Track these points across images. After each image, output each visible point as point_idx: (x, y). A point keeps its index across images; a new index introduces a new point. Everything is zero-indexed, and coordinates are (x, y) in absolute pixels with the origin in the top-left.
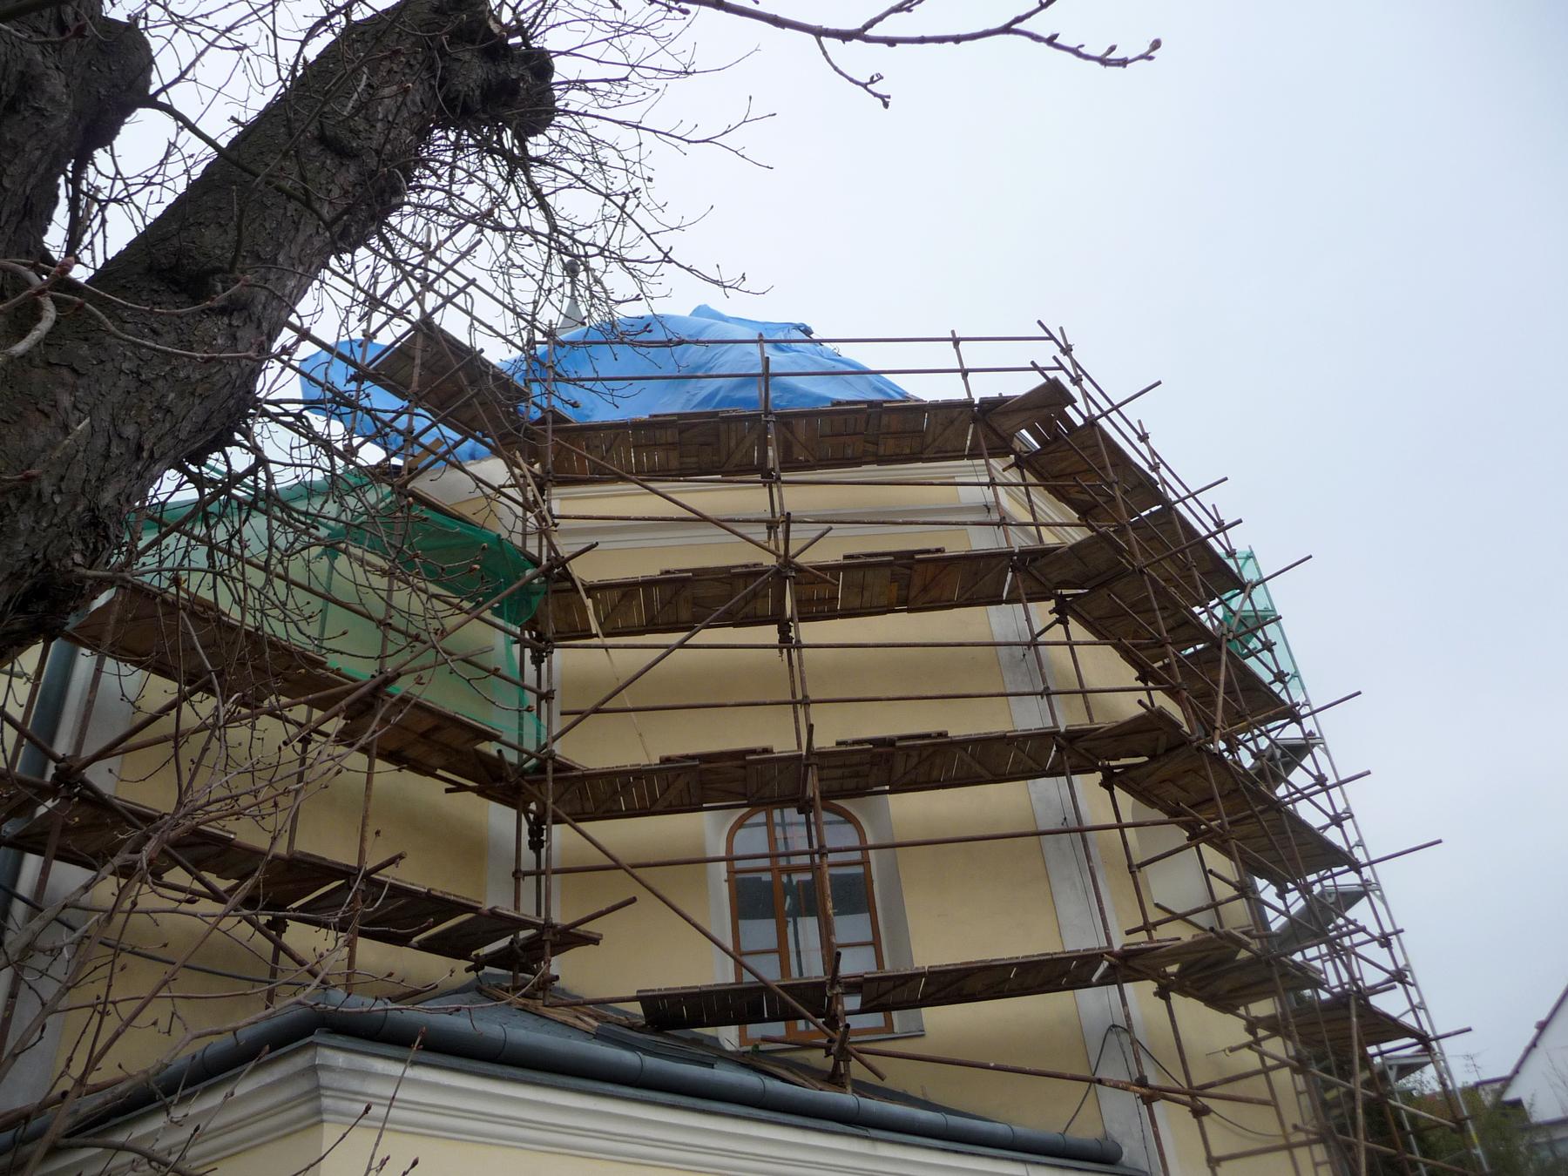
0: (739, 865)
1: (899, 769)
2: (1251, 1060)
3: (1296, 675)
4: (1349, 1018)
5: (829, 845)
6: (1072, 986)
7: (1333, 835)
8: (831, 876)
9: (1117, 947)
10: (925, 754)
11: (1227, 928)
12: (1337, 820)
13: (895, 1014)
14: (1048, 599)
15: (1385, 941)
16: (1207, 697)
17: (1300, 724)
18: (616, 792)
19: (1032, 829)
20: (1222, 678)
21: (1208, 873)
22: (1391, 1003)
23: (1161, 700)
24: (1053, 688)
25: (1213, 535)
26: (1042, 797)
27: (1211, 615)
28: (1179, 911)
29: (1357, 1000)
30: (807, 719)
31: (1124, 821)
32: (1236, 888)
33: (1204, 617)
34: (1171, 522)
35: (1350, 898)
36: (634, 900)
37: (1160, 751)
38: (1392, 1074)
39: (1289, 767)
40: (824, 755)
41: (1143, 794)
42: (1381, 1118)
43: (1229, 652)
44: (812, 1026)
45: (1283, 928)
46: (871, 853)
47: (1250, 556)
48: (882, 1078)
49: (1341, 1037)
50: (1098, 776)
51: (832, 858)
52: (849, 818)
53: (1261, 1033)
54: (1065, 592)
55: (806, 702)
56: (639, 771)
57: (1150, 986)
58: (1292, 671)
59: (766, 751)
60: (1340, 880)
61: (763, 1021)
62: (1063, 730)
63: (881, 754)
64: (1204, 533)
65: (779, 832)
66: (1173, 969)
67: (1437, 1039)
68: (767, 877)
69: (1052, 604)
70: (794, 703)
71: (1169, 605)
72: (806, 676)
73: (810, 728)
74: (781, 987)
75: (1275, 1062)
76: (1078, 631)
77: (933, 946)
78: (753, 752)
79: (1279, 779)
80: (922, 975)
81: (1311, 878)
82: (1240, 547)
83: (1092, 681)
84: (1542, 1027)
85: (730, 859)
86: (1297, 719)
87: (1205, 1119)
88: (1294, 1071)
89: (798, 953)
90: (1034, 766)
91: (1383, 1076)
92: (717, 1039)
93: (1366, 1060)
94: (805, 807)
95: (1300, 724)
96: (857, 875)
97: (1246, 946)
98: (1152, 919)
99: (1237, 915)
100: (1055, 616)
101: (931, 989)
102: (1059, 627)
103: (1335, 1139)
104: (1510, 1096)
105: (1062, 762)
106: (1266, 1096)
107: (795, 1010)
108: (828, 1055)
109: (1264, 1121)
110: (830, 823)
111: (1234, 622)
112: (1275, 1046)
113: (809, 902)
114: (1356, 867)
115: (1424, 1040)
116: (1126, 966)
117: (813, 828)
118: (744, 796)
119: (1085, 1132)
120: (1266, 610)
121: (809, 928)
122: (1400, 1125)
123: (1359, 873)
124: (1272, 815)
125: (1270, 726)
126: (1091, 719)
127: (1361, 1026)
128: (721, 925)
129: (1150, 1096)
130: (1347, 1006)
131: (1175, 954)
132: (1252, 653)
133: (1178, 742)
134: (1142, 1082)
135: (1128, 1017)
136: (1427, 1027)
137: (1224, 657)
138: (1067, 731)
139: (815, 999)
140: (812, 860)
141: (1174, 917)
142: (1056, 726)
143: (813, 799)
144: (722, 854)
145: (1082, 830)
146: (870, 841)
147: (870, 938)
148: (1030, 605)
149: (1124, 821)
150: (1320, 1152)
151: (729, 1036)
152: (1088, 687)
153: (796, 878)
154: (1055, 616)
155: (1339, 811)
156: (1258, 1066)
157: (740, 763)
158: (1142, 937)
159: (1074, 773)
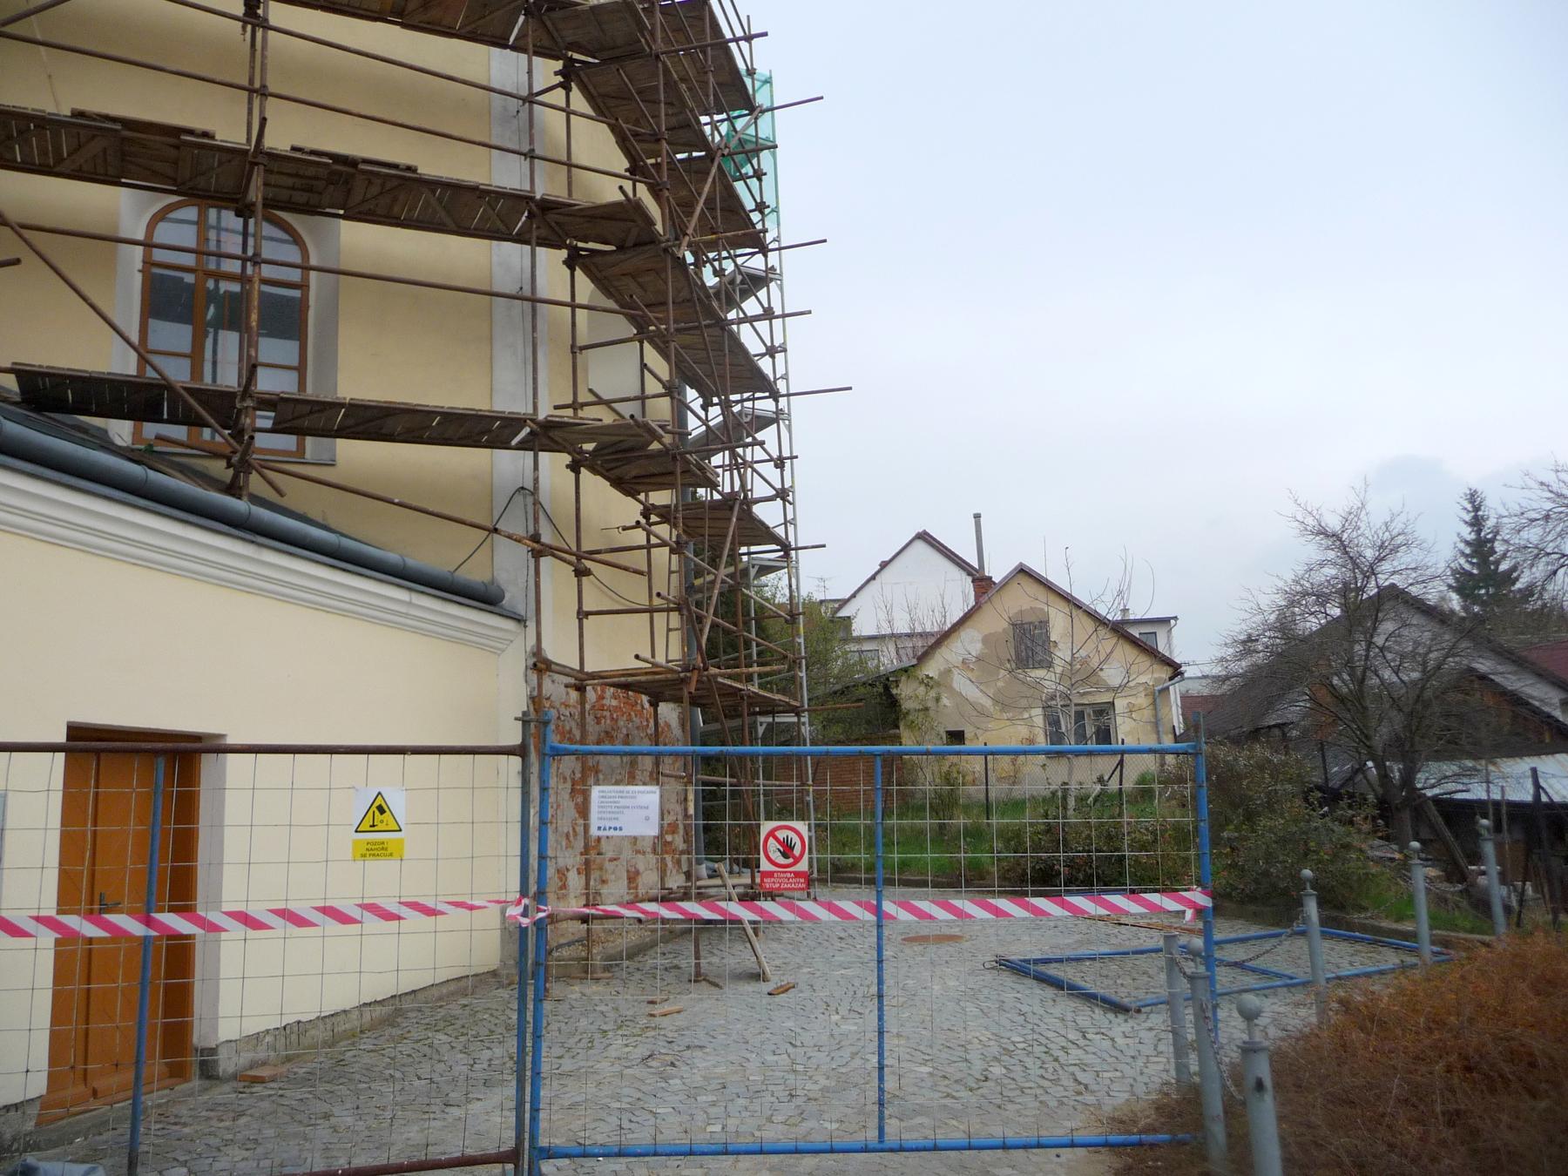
0: (159, 255)
1: (357, 197)
2: (639, 537)
3: (776, 210)
4: (730, 519)
5: (265, 254)
6: (491, 445)
7: (765, 365)
8: (261, 293)
9: (541, 417)
10: (388, 186)
11: (648, 419)
12: (771, 352)
13: (309, 440)
14: (556, 58)
15: (780, 463)
16: (688, 206)
17: (766, 256)
18: (10, 137)
19: (485, 288)
20: (706, 189)
21: (644, 366)
22: (770, 514)
23: (643, 193)
24: (538, 152)
25: (736, 40)
26: (502, 260)
27: (715, 127)
28: (606, 397)
29: (742, 503)
30: (262, 111)
31: (578, 300)
32: (664, 387)
33: (707, 129)
34: (702, 19)
35: (763, 422)
36: (17, 262)
37: (630, 243)
38: (753, 572)
39: (745, 294)
40: (273, 156)
41: (602, 282)
42: (733, 601)
43: (720, 168)
44: (218, 438)
45: (699, 437)
46: (313, 274)
47: (768, 81)
48: (282, 495)
49: (719, 534)
50: (564, 253)
51: (267, 271)
52: (297, 240)
53: (654, 518)
54: (576, 56)
55: (264, 93)
56: (43, 118)
57: (566, 458)
58: (773, 205)
59: (205, 134)
60: (758, 404)
61: (161, 421)
62: (538, 197)
63: (340, 174)
64: (728, 35)
65: (212, 235)
66: (589, 447)
67: (797, 549)
68: (189, 278)
69: (559, 65)
70: (251, 91)
71: (675, 102)
72: (269, 61)
73: (263, 121)
74: (185, 389)
75: (592, 398)
76: (579, 101)
77: (358, 381)
78: (191, 132)
79: (732, 303)
80: (342, 405)
81: (733, 397)
82: (762, 70)
83: (579, 157)
84: (884, 565)
85: (148, 245)
86: (764, 250)
87: (584, 579)
88: (672, 551)
89: (215, 363)
90: (502, 227)
91: (745, 573)
92: (106, 432)
93: (734, 558)
94: (244, 211)
95: (766, 256)
96: (293, 299)
97: (659, 439)
98: (580, 400)
99: (661, 409)
100: (560, 79)
101: (351, 422)
102: (561, 92)
103: (689, 610)
104: (843, 613)
105: (530, 231)
106: (645, 568)
107: (198, 415)
108: (229, 466)
109: (637, 592)
110: (272, 239)
111: (733, 143)
112: (663, 530)
113: (233, 315)
114: (775, 396)
115: (786, 548)
116: (546, 436)
117: (251, 241)
118: (174, 181)
119: (473, 574)
120: (767, 139)
121: (229, 342)
122: (747, 613)
123: (777, 401)
124: (716, 331)
125: (739, 252)
126: (570, 194)
127: (738, 527)
128: (129, 313)
129: (539, 551)
130: (731, 508)
131: (591, 433)
132: (744, 178)
133: (648, 239)
134: (535, 538)
135: (536, 480)
136: (791, 539)
137: (714, 170)
138: (543, 200)
139: (223, 409)
140: (244, 268)
141: (600, 401)
142: (532, 191)
143: (253, 204)
144: (140, 236)
145: (534, 300)
146: (313, 262)
147: (295, 363)
148: (536, 59)
149: (578, 300)
150: (675, 619)
151: (121, 431)
152: (575, 160)
153: (224, 286)
154: (560, 79)
155: (777, 344)
156: (644, 542)
157: (172, 141)
158: (570, 412)
159: (539, 245)
